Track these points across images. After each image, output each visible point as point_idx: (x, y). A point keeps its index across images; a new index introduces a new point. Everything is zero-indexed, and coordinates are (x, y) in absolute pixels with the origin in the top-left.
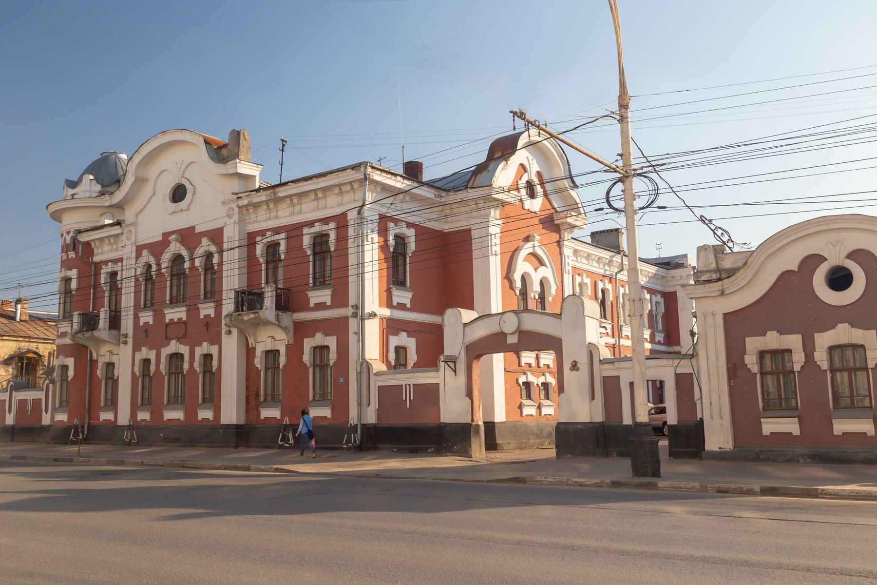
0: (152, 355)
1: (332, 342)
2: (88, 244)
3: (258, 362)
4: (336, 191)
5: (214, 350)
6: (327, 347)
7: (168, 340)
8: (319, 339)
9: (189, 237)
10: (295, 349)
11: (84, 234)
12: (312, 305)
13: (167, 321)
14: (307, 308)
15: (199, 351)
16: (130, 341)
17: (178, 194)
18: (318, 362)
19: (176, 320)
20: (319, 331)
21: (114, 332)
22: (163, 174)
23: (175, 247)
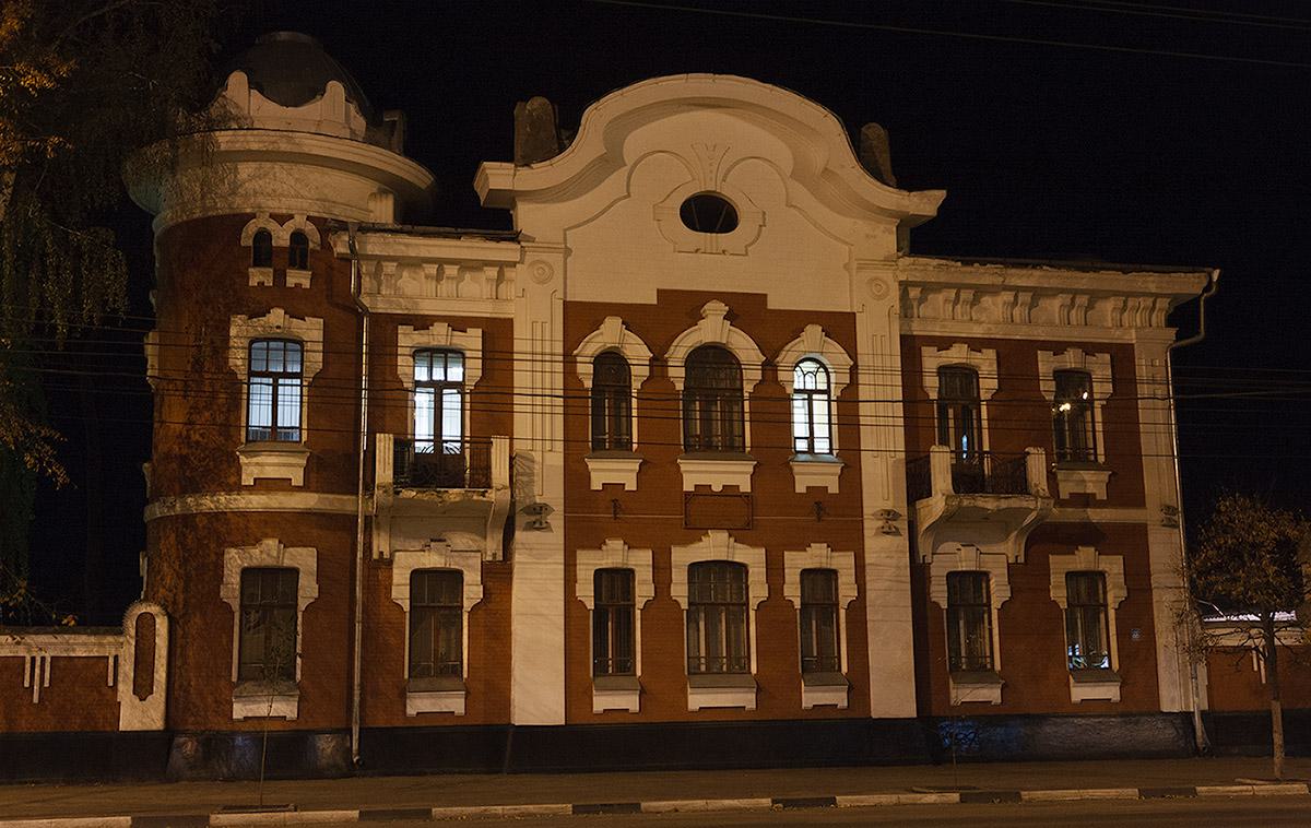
1: (1113, 566)
3: (939, 594)
4: (432, 269)
7: (693, 531)
8: (1084, 558)
10: (1027, 576)
11: (373, 238)
12: (247, 480)
13: (688, 486)
14: (239, 488)
16: (556, 520)
17: (709, 214)
19: (717, 488)
20: (614, 536)
23: (712, 328)
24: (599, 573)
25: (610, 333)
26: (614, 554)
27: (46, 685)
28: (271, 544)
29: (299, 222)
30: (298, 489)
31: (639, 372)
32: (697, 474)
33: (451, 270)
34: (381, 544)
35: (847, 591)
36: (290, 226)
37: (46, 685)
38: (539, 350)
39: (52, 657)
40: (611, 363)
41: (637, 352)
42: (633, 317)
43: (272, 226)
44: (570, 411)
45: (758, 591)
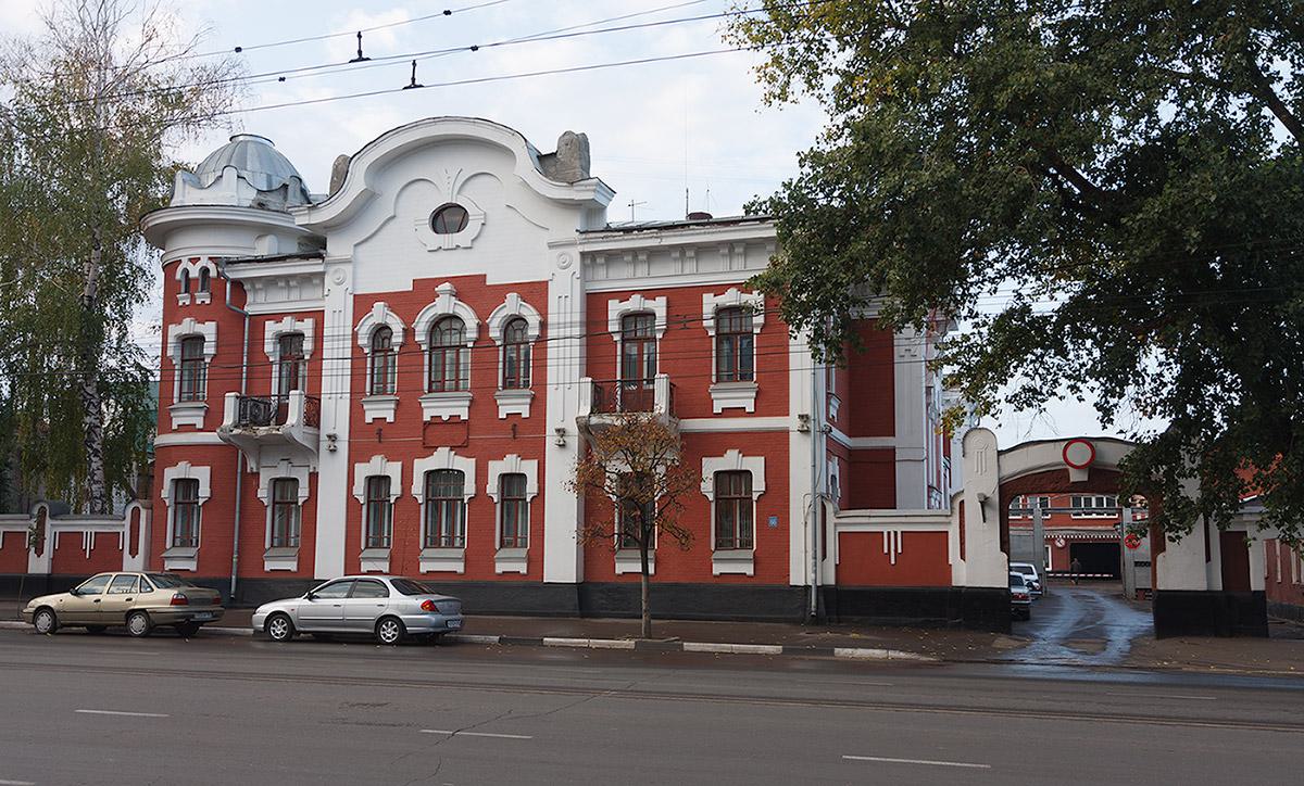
0: (394, 470)
1: (756, 465)
2: (238, 285)
5: (529, 468)
6: (196, 481)
7: (428, 450)
8: (731, 460)
9: (471, 289)
12: (175, 427)
13: (427, 418)
15: (496, 468)
18: (277, 499)
19: (445, 418)
20: (733, 448)
21: (310, 430)
22: (486, 178)
23: (444, 304)
24: (717, 474)
25: (379, 313)
26: (376, 465)
27: (900, 551)
28: (182, 464)
29: (204, 262)
30: (750, 414)
31: (397, 339)
32: (432, 408)
33: (690, 253)
34: (252, 465)
35: (532, 488)
36: (199, 265)
37: (900, 551)
38: (342, 333)
39: (96, 533)
40: (381, 331)
41: (397, 325)
42: (395, 301)
43: (190, 266)
44: (356, 371)
45: (469, 488)
